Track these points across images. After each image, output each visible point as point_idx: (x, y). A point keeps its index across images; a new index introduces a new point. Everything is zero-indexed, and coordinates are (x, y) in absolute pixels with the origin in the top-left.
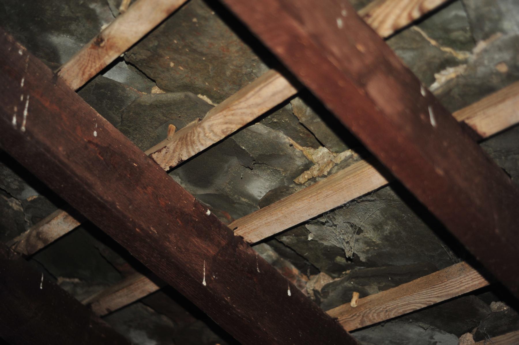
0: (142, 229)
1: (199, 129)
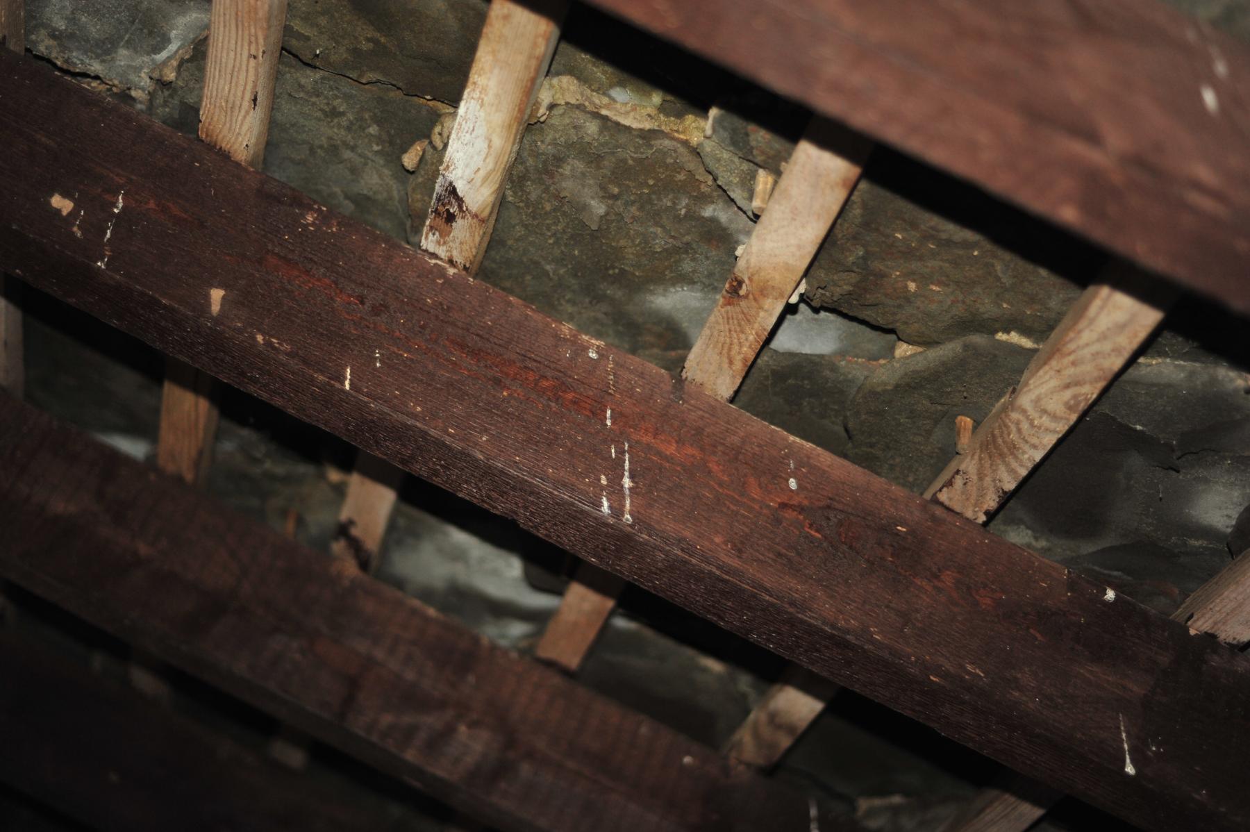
0: (945, 675)
1: (1015, 415)
